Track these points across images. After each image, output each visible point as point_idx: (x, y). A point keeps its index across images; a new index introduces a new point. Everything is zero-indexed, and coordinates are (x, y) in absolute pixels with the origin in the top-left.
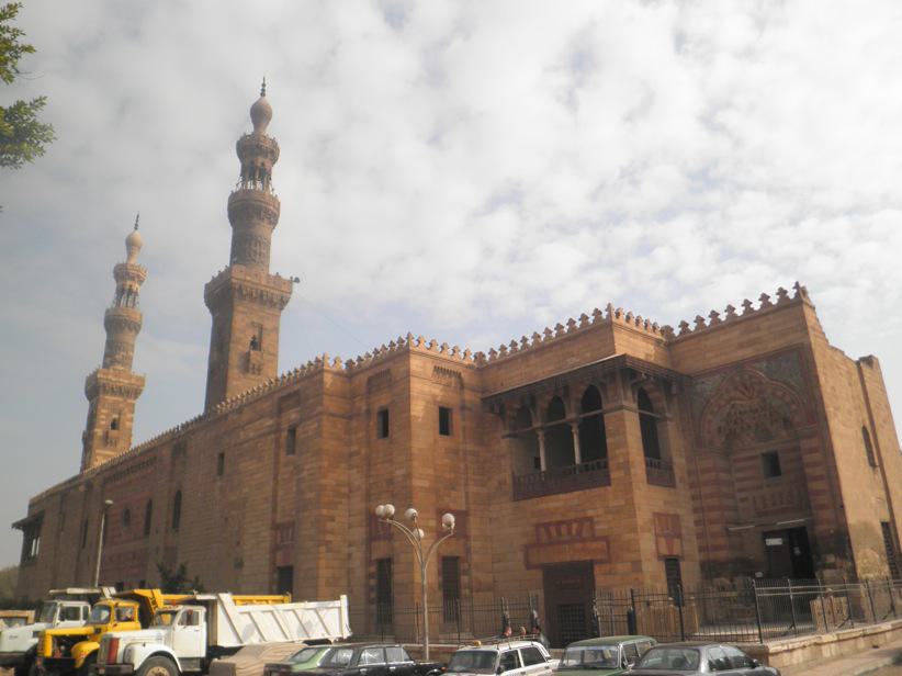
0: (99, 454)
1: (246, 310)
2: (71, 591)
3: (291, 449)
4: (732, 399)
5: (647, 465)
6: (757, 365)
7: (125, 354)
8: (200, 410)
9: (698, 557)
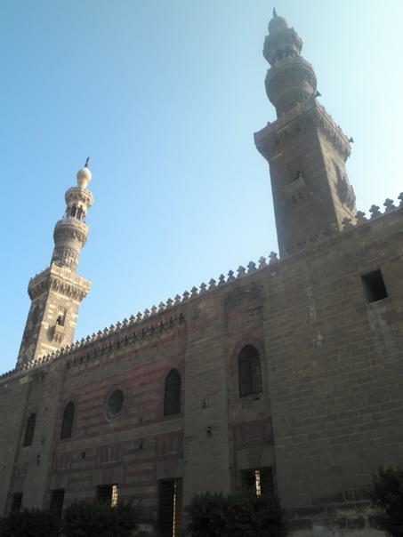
0: (44, 348)
7: (73, 259)
8: (12, 367)
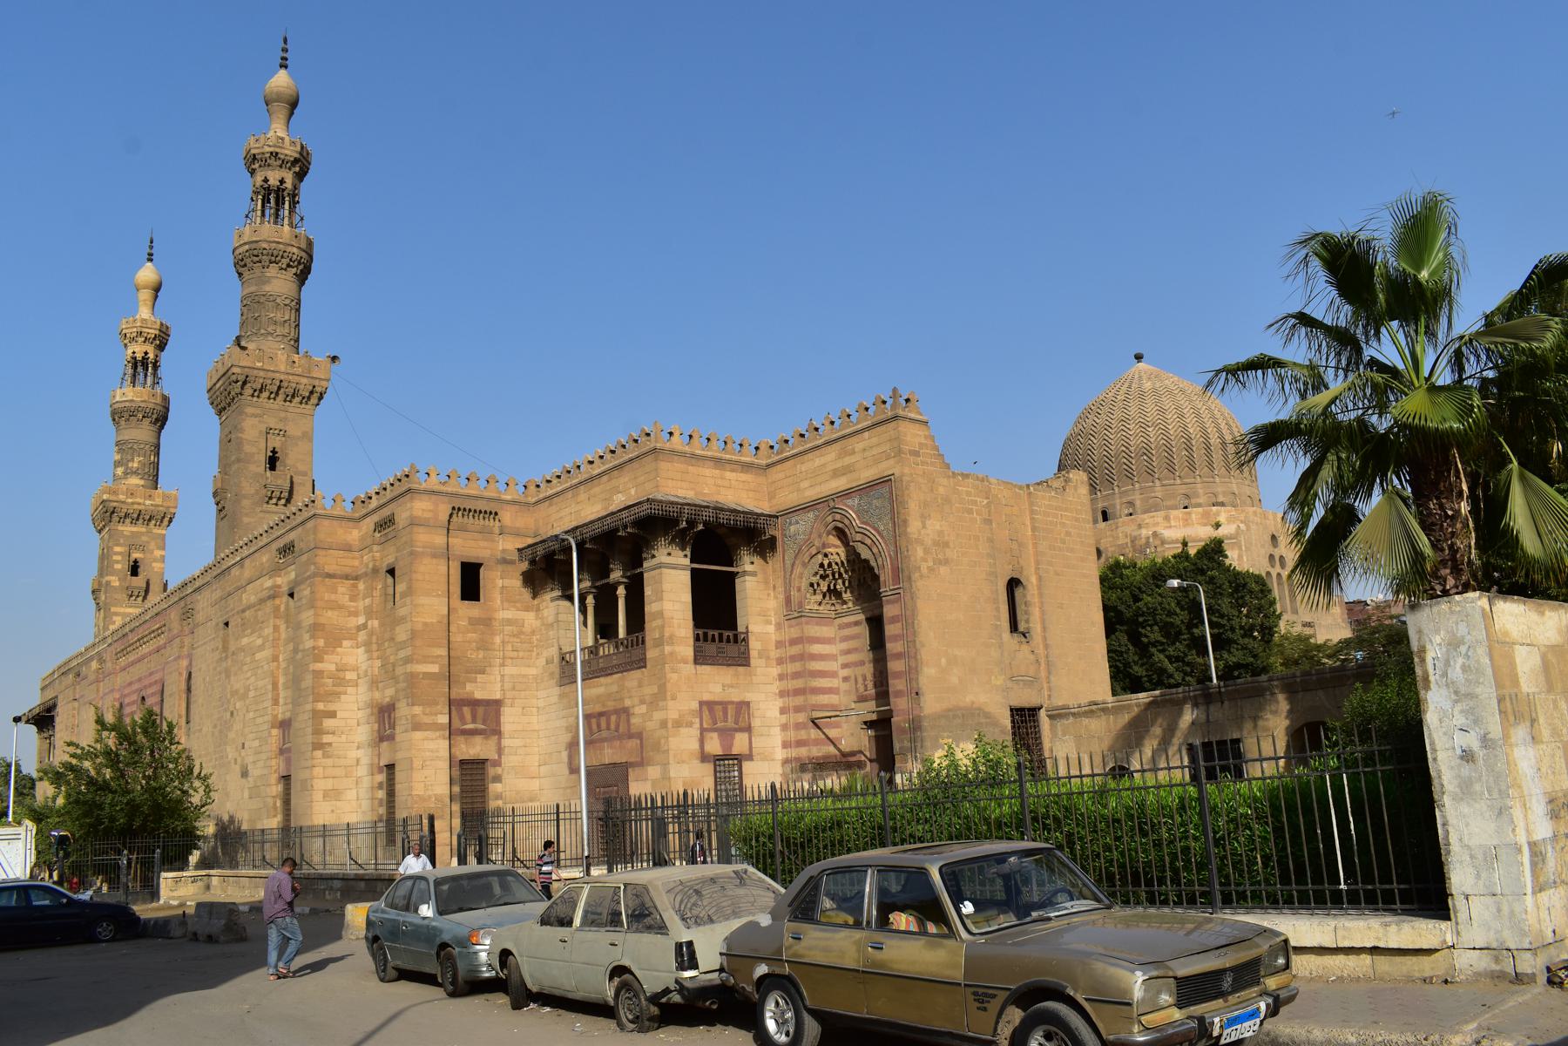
0: (116, 614)
1: (258, 411)
2: (714, 835)
3: (837, 529)
4: (824, 546)
5: (697, 638)
6: (849, 502)
9: (780, 754)
